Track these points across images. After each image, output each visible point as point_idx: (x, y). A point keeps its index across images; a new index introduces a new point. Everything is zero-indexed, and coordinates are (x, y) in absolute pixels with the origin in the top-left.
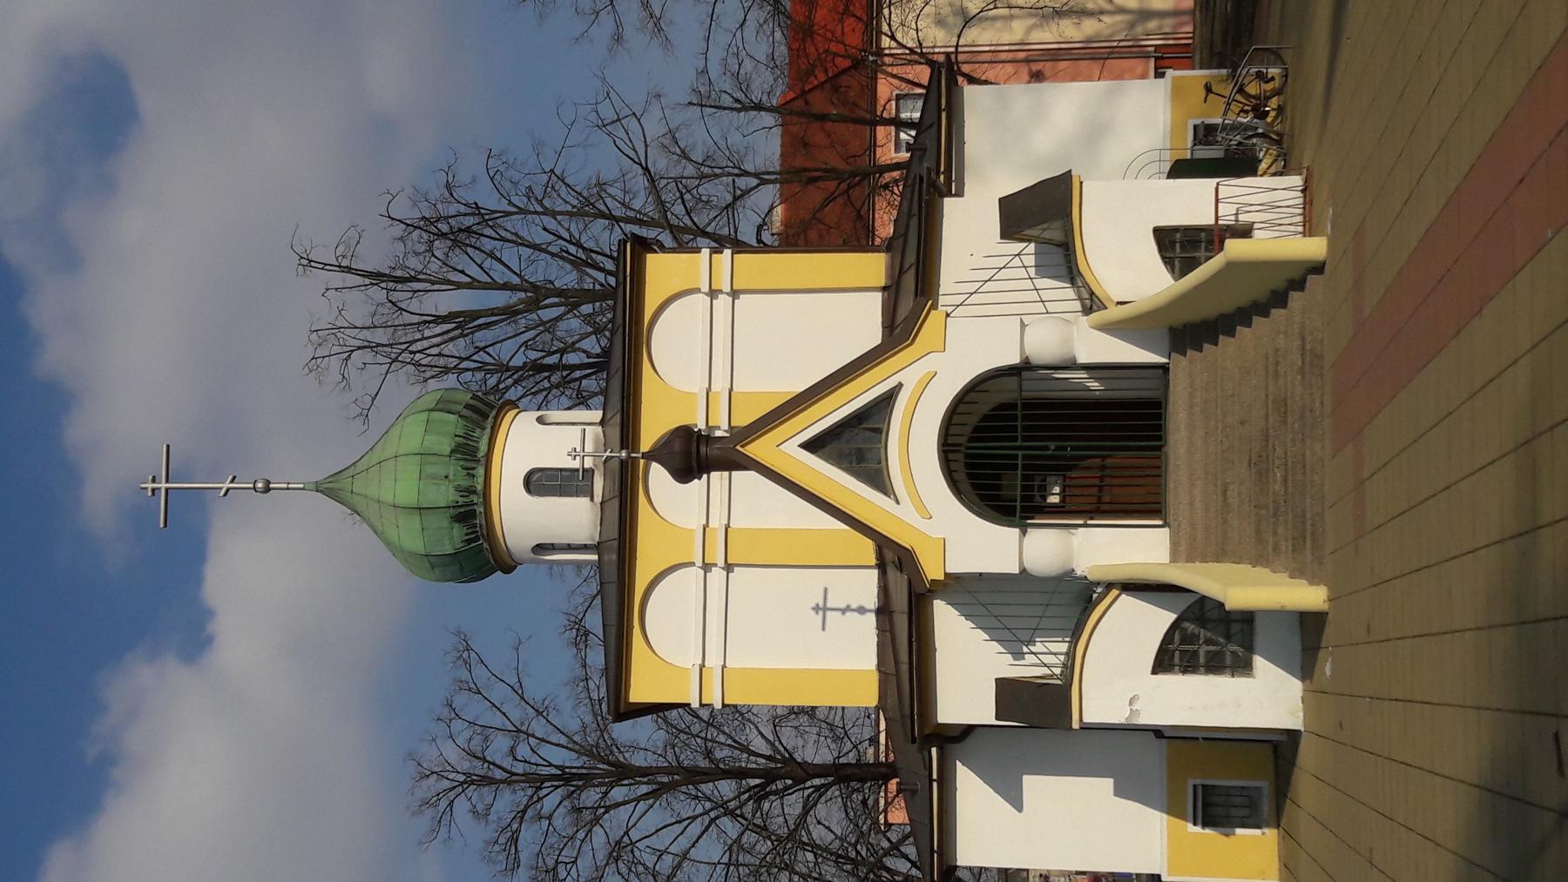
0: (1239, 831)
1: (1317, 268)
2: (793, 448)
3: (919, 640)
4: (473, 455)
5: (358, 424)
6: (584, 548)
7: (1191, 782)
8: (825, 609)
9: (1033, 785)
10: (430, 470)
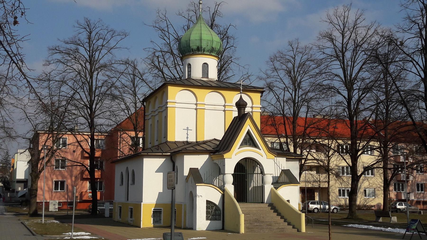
0: (152, 219)
1: (299, 230)
2: (248, 128)
3: (202, 152)
4: (211, 52)
5: (178, 13)
6: (189, 75)
7: (162, 209)
8: (188, 130)
9: (161, 175)
10: (209, 43)
